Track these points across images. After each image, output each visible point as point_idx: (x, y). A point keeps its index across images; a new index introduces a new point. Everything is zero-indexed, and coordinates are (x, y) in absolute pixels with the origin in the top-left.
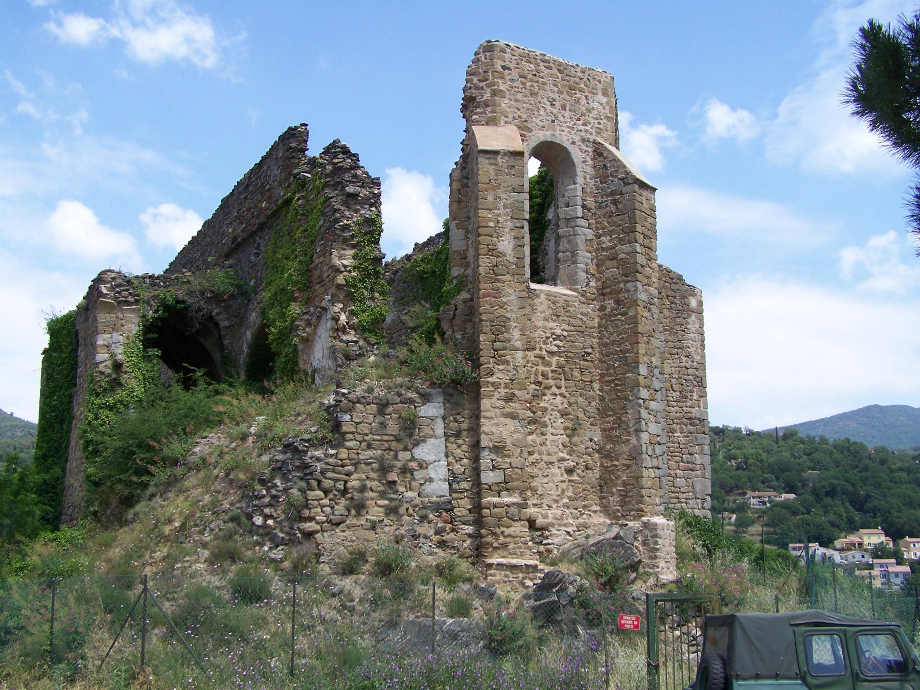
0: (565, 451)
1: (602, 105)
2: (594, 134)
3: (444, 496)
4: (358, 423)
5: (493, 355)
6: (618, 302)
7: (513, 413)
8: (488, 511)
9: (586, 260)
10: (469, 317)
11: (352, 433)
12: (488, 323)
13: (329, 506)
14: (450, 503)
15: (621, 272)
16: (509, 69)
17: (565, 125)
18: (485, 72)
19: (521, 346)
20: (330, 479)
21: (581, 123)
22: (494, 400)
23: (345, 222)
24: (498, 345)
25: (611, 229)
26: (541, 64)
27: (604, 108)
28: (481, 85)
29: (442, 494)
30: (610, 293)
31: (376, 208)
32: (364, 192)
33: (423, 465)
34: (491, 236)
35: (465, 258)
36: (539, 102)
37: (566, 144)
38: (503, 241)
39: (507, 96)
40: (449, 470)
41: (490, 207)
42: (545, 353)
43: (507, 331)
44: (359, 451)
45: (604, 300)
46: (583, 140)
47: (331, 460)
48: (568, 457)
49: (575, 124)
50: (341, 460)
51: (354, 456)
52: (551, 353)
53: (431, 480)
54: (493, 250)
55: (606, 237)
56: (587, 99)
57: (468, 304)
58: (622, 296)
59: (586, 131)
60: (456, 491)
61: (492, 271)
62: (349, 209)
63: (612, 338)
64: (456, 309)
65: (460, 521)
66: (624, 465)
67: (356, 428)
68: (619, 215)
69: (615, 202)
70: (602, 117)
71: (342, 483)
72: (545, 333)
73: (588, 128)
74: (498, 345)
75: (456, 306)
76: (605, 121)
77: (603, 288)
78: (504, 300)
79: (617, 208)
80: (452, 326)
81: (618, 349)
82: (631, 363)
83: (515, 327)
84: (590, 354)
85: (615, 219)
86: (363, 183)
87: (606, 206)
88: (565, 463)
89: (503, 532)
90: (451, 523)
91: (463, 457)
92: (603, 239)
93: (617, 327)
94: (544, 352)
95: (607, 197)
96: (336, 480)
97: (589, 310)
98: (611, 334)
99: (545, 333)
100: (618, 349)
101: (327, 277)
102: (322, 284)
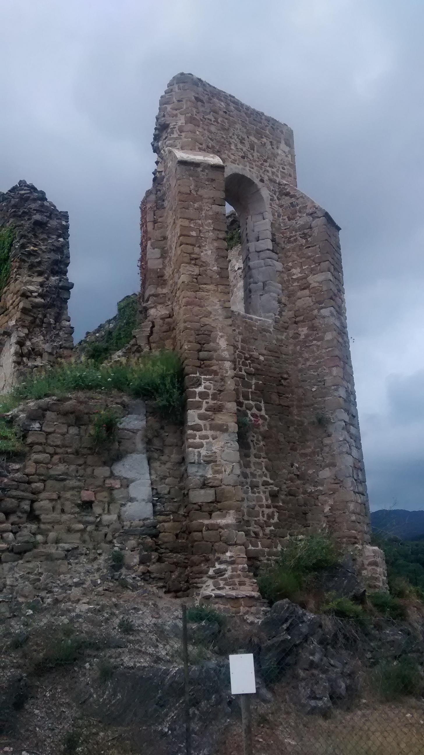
0: (268, 476)
1: (284, 152)
2: (280, 176)
3: (148, 519)
4: (48, 434)
5: (199, 365)
6: (313, 328)
7: (222, 425)
8: (199, 534)
9: (278, 290)
10: (168, 333)
11: (41, 444)
12: (192, 331)
13: (11, 531)
14: (155, 527)
15: (314, 300)
16: (202, 101)
17: (254, 163)
18: (179, 101)
19: (228, 356)
20: (13, 497)
21: (267, 164)
22: (203, 411)
23: (32, 248)
24: (202, 354)
25: (301, 261)
26: (231, 104)
27: (287, 156)
28: (175, 112)
29: (145, 516)
30: (303, 321)
31: (64, 239)
32: (53, 223)
33: (126, 483)
34: (194, 245)
35: (162, 276)
36: (231, 137)
37: (257, 181)
38: (206, 250)
39: (201, 125)
40: (153, 489)
41: (192, 217)
42: (245, 374)
43: (214, 341)
44: (50, 466)
45: (298, 327)
46: (271, 180)
47: (16, 475)
48: (271, 481)
49: (262, 164)
50: (28, 475)
51: (42, 470)
52: (249, 374)
53: (131, 500)
54: (196, 259)
55: (296, 268)
56: (272, 145)
57: (167, 320)
58: (317, 322)
59: (273, 173)
60: (161, 513)
61: (195, 280)
62: (36, 236)
63: (308, 364)
64: (153, 326)
65: (166, 548)
66: (330, 489)
67: (46, 439)
68: (309, 247)
69: (305, 236)
70: (286, 164)
71: (28, 502)
72: (244, 354)
73: (274, 170)
74: (202, 354)
75: (153, 323)
76: (288, 167)
77: (296, 317)
78: (209, 309)
79: (307, 241)
80: (149, 343)
81: (316, 374)
82: (330, 387)
83: (221, 337)
84: (286, 379)
85: (306, 251)
86: (51, 214)
87: (296, 240)
88: (269, 488)
89: (219, 558)
90: (156, 550)
91: (168, 474)
92: (294, 271)
93: (313, 352)
94: (243, 373)
95: (296, 232)
96: (21, 499)
97: (283, 337)
98: (307, 360)
99: (244, 354)
100: (316, 374)
101: (12, 304)
102: (6, 313)
